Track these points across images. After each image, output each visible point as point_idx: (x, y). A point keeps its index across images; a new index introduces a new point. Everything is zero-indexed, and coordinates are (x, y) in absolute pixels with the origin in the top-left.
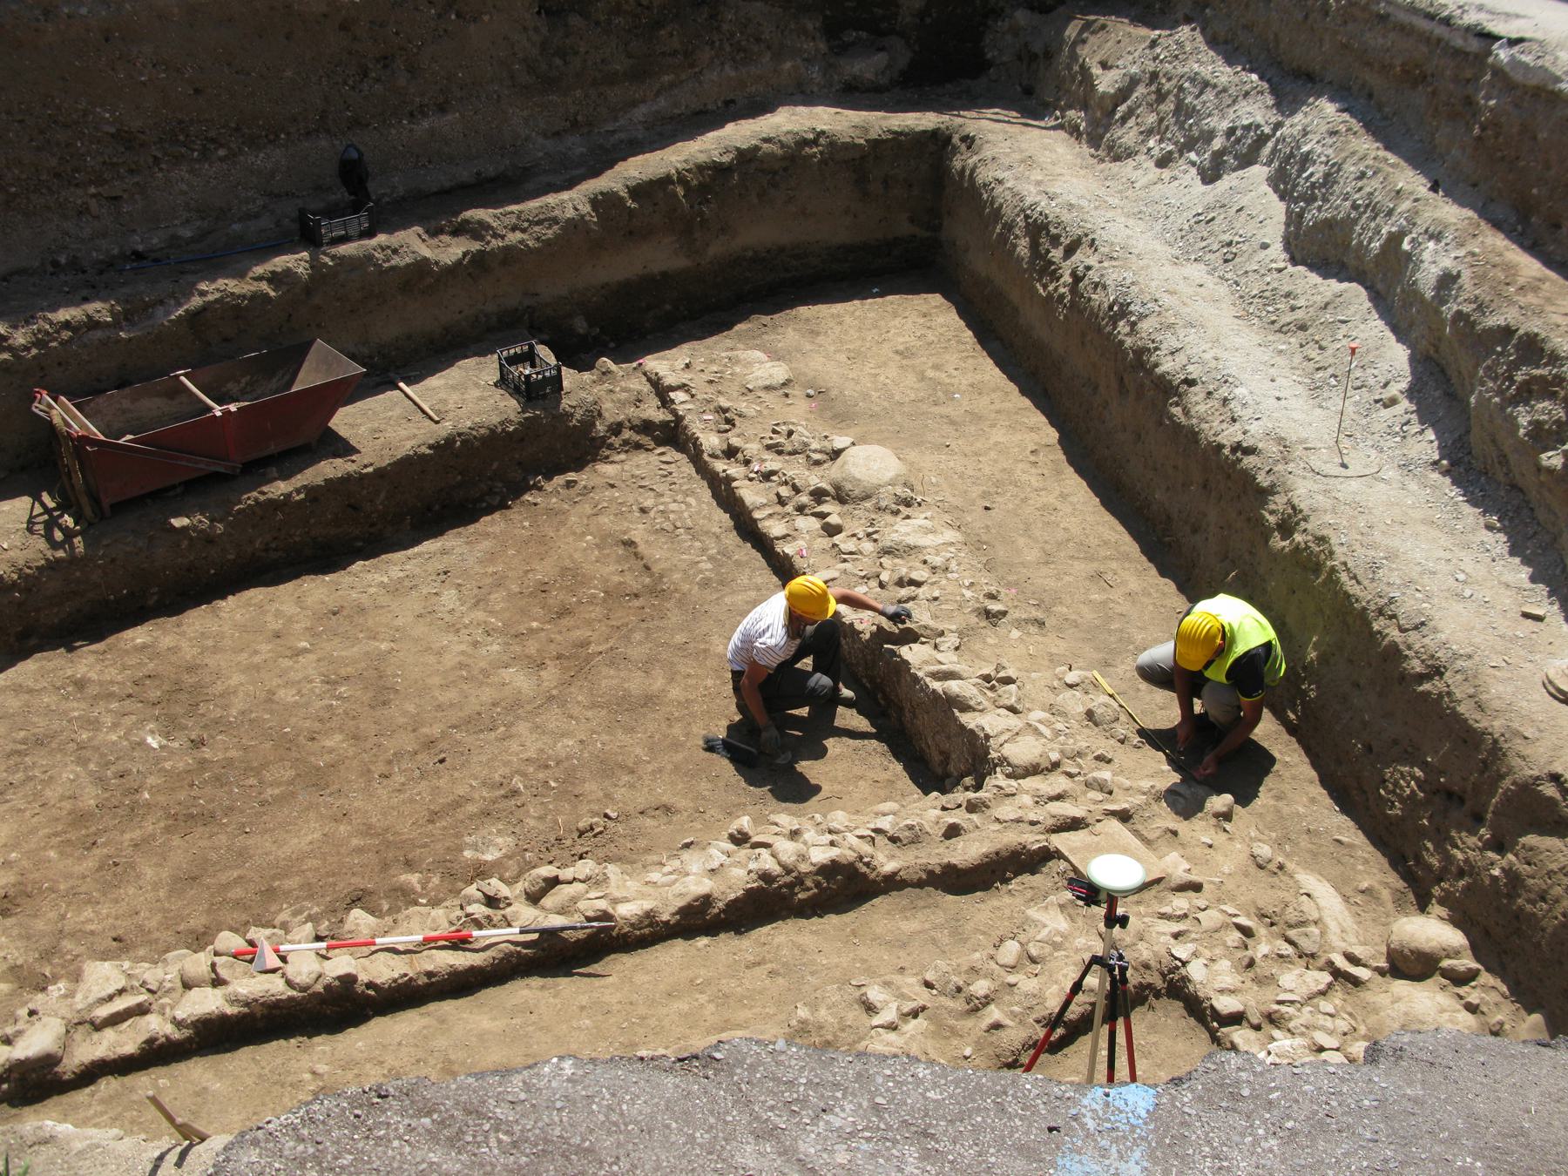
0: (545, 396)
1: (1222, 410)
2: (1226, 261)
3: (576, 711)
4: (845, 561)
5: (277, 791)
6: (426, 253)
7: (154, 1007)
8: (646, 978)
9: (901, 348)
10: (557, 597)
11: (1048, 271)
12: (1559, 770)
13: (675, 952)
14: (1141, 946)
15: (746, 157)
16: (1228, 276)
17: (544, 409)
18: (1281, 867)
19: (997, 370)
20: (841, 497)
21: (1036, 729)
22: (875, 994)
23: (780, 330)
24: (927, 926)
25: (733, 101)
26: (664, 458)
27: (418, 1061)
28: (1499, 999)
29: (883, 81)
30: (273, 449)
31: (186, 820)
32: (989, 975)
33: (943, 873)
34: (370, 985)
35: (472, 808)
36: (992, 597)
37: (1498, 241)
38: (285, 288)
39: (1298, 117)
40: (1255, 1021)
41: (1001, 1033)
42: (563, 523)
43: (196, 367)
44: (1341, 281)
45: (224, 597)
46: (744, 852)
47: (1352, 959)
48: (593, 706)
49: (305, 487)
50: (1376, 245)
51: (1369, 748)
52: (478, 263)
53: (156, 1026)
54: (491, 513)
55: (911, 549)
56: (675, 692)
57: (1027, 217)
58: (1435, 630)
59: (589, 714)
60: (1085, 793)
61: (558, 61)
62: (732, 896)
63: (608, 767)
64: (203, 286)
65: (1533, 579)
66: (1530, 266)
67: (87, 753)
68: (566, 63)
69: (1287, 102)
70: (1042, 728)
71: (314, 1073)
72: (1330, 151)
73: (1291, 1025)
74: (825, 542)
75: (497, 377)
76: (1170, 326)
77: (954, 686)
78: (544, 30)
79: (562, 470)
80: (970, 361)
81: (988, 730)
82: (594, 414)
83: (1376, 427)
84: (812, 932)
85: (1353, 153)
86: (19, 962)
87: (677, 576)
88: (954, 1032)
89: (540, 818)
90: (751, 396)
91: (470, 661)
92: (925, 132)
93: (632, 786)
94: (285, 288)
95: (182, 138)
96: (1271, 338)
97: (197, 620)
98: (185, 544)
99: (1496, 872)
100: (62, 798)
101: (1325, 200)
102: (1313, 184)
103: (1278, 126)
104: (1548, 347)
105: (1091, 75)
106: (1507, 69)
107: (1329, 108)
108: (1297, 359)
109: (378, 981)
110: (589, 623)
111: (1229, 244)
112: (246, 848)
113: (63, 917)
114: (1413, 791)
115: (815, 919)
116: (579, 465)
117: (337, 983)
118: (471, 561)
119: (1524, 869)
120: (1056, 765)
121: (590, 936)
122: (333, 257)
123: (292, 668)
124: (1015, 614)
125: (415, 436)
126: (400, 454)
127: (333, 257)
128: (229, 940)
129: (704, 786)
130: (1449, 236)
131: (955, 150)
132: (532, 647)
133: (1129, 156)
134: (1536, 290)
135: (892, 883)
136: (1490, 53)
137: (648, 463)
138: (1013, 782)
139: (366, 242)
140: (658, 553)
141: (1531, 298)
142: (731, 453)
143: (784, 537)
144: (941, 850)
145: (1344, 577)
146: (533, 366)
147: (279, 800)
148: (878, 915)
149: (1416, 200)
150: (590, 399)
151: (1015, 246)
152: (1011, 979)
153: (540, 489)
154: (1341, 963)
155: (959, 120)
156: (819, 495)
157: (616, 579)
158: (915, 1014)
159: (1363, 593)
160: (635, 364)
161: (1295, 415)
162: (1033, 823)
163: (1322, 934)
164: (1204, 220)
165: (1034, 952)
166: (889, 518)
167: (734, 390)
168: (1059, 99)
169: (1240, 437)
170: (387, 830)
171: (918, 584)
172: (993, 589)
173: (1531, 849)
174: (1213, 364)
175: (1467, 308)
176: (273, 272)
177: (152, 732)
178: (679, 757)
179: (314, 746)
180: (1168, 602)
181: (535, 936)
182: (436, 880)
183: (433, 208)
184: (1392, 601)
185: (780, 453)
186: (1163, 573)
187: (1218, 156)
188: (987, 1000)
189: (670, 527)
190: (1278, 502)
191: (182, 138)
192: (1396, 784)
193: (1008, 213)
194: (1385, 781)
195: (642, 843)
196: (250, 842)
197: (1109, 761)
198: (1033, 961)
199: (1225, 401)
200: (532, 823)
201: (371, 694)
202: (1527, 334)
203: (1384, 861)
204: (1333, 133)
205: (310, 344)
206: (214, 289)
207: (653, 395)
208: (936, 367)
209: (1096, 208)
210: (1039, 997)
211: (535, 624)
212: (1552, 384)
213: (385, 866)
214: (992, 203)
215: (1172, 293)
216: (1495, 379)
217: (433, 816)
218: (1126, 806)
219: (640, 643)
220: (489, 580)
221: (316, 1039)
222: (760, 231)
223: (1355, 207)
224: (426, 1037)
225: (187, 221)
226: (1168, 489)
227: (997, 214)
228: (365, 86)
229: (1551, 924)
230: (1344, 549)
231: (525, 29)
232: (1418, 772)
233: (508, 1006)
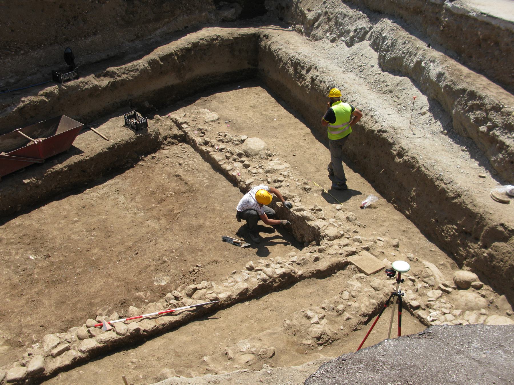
0: (142, 129)
1: (371, 119)
2: (360, 72)
3: (177, 233)
4: (254, 176)
5: (81, 270)
6: (96, 83)
7: (71, 347)
8: (232, 317)
9: (252, 105)
10: (158, 195)
11: (302, 78)
12: (503, 222)
13: (239, 308)
14: (385, 288)
15: (195, 45)
16: (362, 76)
17: (142, 133)
18: (417, 260)
19: (285, 110)
20: (247, 155)
21: (333, 225)
22: (310, 313)
23: (211, 102)
24: (315, 290)
25: (187, 27)
26: (183, 147)
27: (166, 354)
28: (490, 292)
29: (234, 18)
30: (55, 153)
31: (52, 283)
32: (342, 303)
33: (317, 273)
34: (145, 331)
35: (151, 268)
36: (305, 184)
37: (452, 62)
38: (51, 98)
39: (378, 25)
40: (423, 307)
41: (350, 320)
42: (154, 171)
43: (23, 127)
44: (401, 76)
45: (44, 205)
46: (253, 273)
47: (446, 286)
48: (182, 230)
49: (67, 166)
50: (412, 65)
51: (437, 221)
52: (113, 86)
53: (74, 354)
54: (129, 169)
55: (276, 170)
56: (208, 223)
57: (292, 60)
58: (456, 183)
59: (182, 233)
60: (353, 243)
61: (131, 16)
62: (254, 288)
63: (193, 250)
64: (23, 99)
65: (480, 165)
66: (465, 70)
67: (10, 264)
68: (134, 16)
69: (374, 20)
70: (334, 224)
71: (132, 362)
72: (392, 36)
73: (434, 307)
74: (245, 170)
75: (124, 124)
76: (349, 93)
77: (305, 213)
78: (126, 6)
79: (150, 154)
80: (276, 108)
81: (319, 226)
82: (158, 134)
83: (420, 122)
84: (281, 296)
85: (400, 36)
86: (9, 338)
87: (197, 185)
88: (335, 322)
89: (176, 269)
90: (207, 124)
91: (135, 220)
92: (251, 34)
93: (203, 255)
94: (51, 98)
95: (8, 47)
96: (381, 95)
97: (36, 214)
98: (29, 189)
99: (486, 255)
100: (6, 280)
101: (393, 51)
102: (388, 47)
103: (371, 28)
104: (478, 94)
105: (305, 14)
106: (451, 9)
107: (389, 22)
108: (391, 102)
109: (147, 329)
110: (172, 203)
111: (361, 66)
112: (78, 290)
113: (20, 321)
114: (454, 233)
115: (280, 292)
116: (155, 152)
117: (134, 331)
118: (126, 186)
119: (495, 253)
120: (342, 235)
121: (212, 306)
122: (66, 87)
123: (74, 227)
124: (314, 189)
125: (101, 145)
126: (98, 152)
127: (66, 87)
128: (91, 322)
129: (226, 253)
130: (438, 61)
131: (262, 40)
132: (155, 213)
133: (320, 39)
134: (470, 77)
135: (302, 278)
136: (444, 4)
137: (178, 148)
138: (330, 242)
139: (76, 81)
140: (189, 178)
141: (468, 80)
142: (206, 143)
143: (231, 170)
144: (314, 266)
145: (423, 169)
146: (136, 119)
147: (82, 273)
148: (299, 288)
149: (424, 50)
150: (157, 129)
151: (288, 70)
152: (349, 303)
153: (144, 160)
154: (443, 287)
155: (262, 30)
156: (240, 155)
157: (177, 188)
158: (323, 318)
159: (431, 174)
160: (167, 116)
161: (395, 119)
162: (341, 254)
163: (435, 279)
164: (350, 59)
165: (353, 294)
166: (265, 161)
167: (201, 122)
168: (293, 22)
169: (380, 128)
170: (125, 279)
171: (281, 181)
172: (306, 181)
173: (496, 247)
174: (366, 105)
175: (449, 84)
176: (46, 93)
177: (31, 254)
178: (215, 244)
179: (90, 253)
180: (359, 181)
181: (195, 308)
182: (149, 293)
183: (98, 67)
184: (441, 175)
185: (223, 142)
186: (355, 172)
187: (352, 38)
188: (343, 311)
189: (191, 170)
190: (397, 147)
191: (8, 47)
192: (447, 231)
193: (285, 59)
194: (443, 231)
195: (212, 274)
196: (79, 288)
197: (358, 232)
198: (354, 297)
199: (372, 116)
200: (173, 271)
201: (104, 234)
202: (470, 91)
203: (446, 255)
204: (392, 30)
205: (60, 117)
206: (27, 100)
207: (175, 126)
208: (265, 111)
209: (314, 56)
210: (359, 308)
211: (154, 205)
212: (481, 106)
213: (129, 291)
214: (278, 56)
215: (347, 83)
216: (461, 105)
217: (140, 272)
218: (367, 246)
219: (192, 208)
220: (134, 192)
221: (129, 351)
222: (200, 70)
223: (403, 53)
224: (166, 346)
225: (12, 76)
226: (354, 145)
227: (280, 60)
228: (69, 27)
229: (505, 269)
230: (422, 160)
231: (120, 5)
232: (455, 227)
233: (190, 332)
